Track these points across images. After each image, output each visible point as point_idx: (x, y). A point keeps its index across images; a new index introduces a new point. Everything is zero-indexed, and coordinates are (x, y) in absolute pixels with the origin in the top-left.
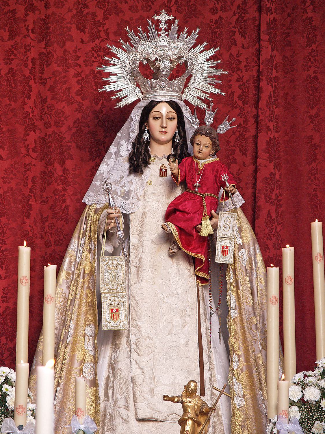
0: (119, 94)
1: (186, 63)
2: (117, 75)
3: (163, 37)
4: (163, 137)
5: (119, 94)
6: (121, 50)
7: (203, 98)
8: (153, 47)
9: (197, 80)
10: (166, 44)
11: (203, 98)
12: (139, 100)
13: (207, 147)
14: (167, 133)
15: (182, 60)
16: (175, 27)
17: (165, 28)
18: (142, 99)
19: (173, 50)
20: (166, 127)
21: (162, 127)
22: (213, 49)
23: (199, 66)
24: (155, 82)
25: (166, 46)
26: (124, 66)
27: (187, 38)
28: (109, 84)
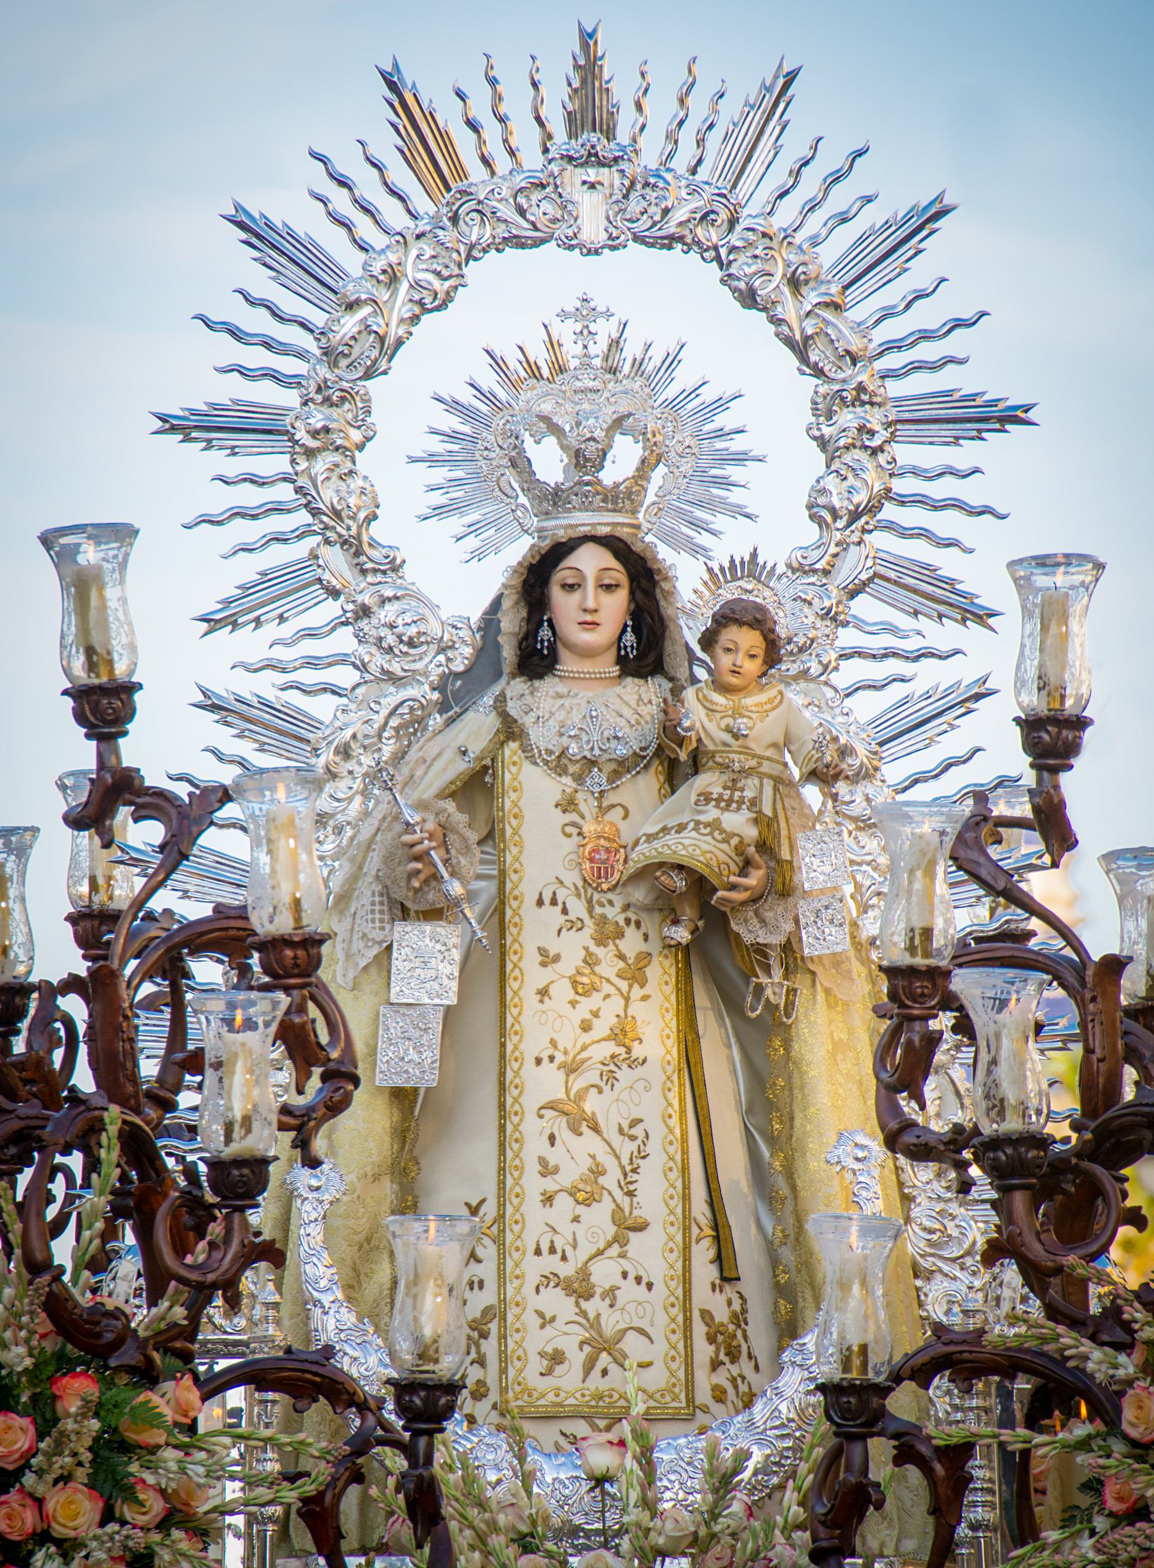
13: (753, 656)
21: (585, 610)
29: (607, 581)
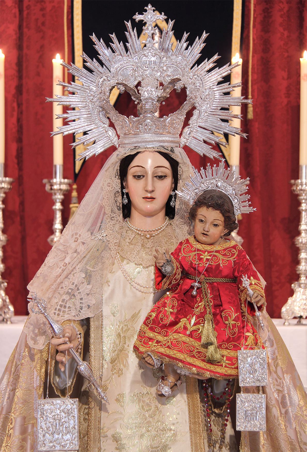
1: (184, 89)
7: (213, 142)
9: (203, 114)
11: (213, 142)
12: (113, 149)
13: (216, 225)
14: (155, 201)
15: (178, 86)
18: (118, 146)
20: (153, 191)
21: (147, 191)
27: (187, 49)
29: (160, 174)
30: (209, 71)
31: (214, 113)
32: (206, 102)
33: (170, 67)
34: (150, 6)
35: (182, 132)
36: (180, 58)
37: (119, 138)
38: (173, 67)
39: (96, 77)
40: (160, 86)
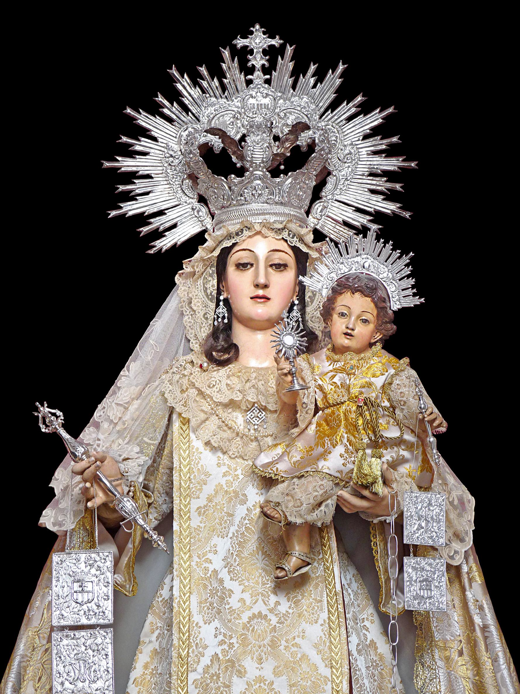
0: (157, 223)
2: (152, 178)
3: (259, 86)
4: (260, 311)
5: (157, 223)
6: (159, 120)
8: (236, 109)
9: (342, 182)
10: (267, 101)
13: (365, 321)
14: (269, 303)
15: (304, 139)
16: (286, 64)
17: (263, 65)
19: (282, 115)
21: (257, 286)
22: (378, 110)
23: (347, 152)
24: (240, 183)
25: (266, 107)
26: (168, 155)
27: (314, 86)
28: (133, 199)
29: (277, 262)
30: (350, 119)
31: (360, 181)
32: (347, 165)
33: (290, 113)
34: (257, 27)
35: (310, 207)
36: (304, 99)
37: (213, 219)
38: (294, 112)
39: (177, 129)
40: (275, 141)
